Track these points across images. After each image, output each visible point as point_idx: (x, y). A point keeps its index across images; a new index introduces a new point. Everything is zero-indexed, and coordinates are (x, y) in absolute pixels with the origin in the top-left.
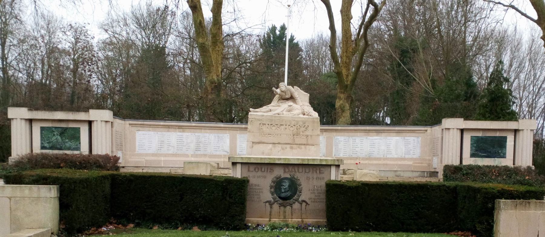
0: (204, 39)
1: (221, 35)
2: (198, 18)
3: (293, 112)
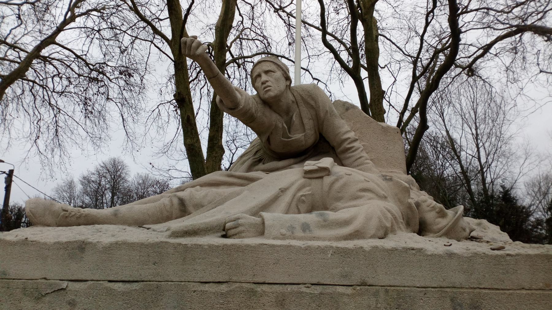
0: (193, 139)
1: (220, 139)
2: (186, 114)
3: (342, 214)
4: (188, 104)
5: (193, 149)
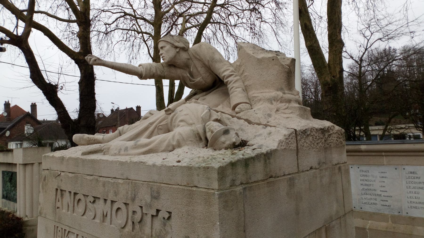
0: (312, 41)
2: (303, 22)
4: (305, 13)
5: (312, 49)
